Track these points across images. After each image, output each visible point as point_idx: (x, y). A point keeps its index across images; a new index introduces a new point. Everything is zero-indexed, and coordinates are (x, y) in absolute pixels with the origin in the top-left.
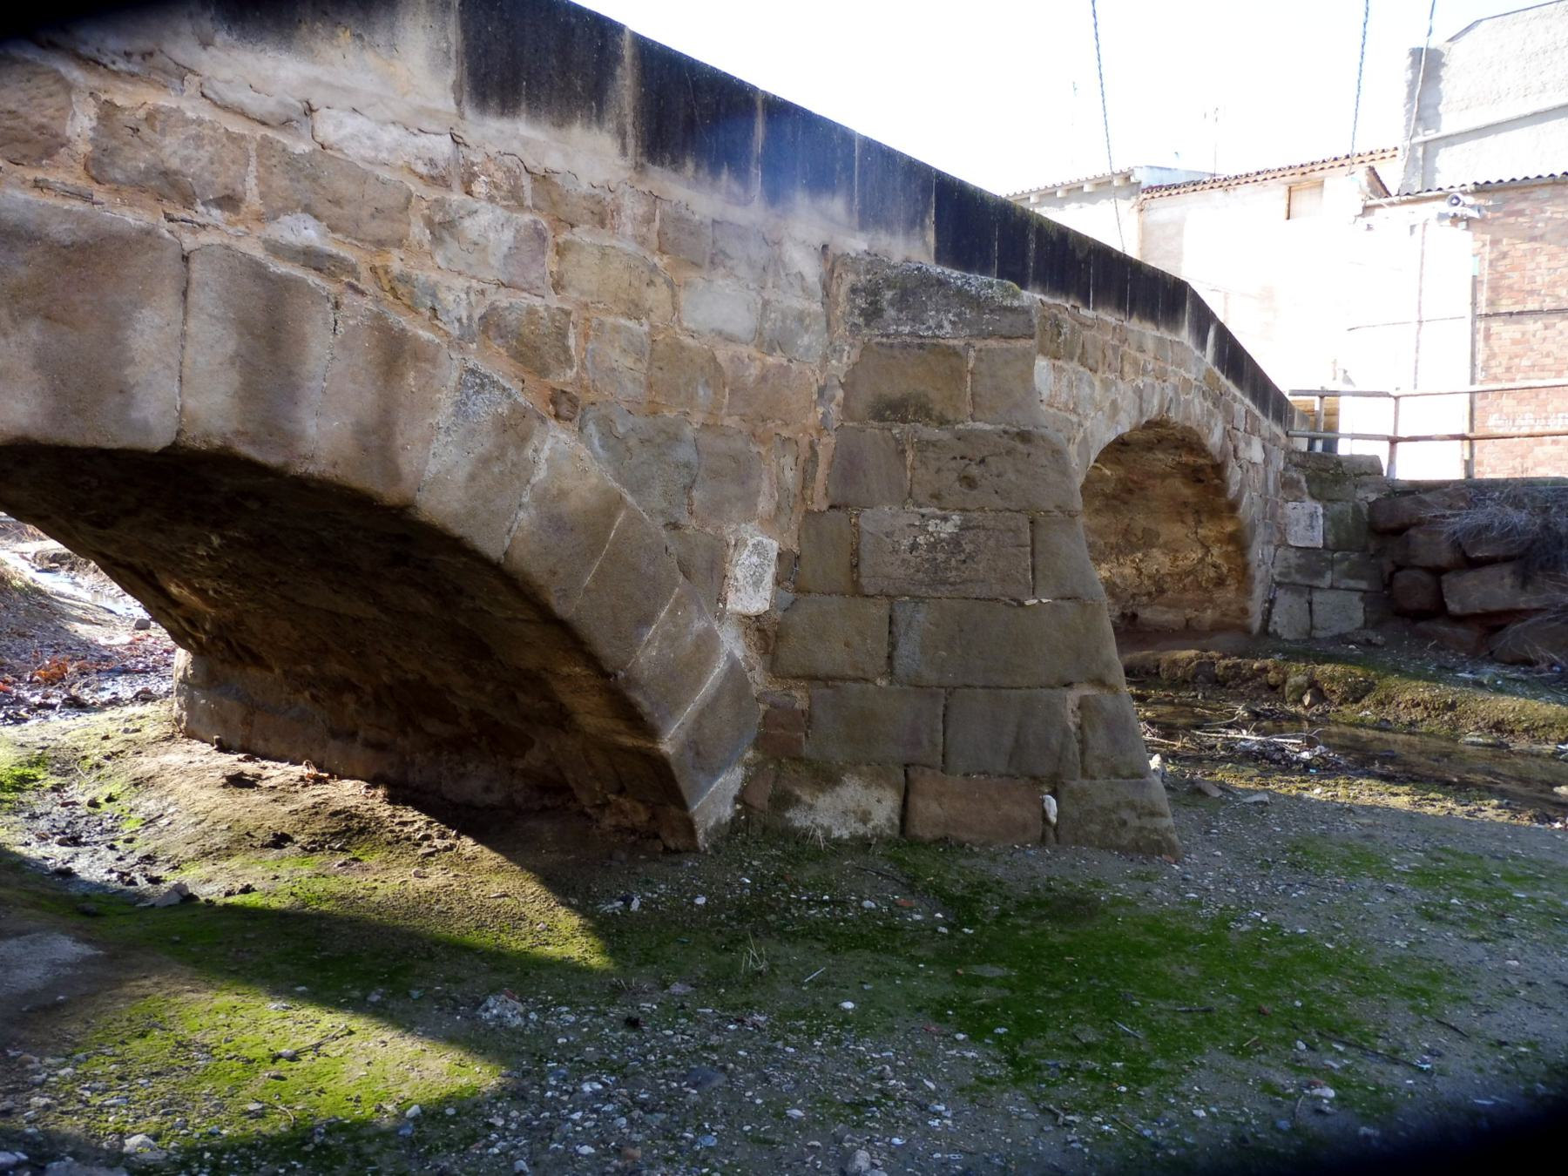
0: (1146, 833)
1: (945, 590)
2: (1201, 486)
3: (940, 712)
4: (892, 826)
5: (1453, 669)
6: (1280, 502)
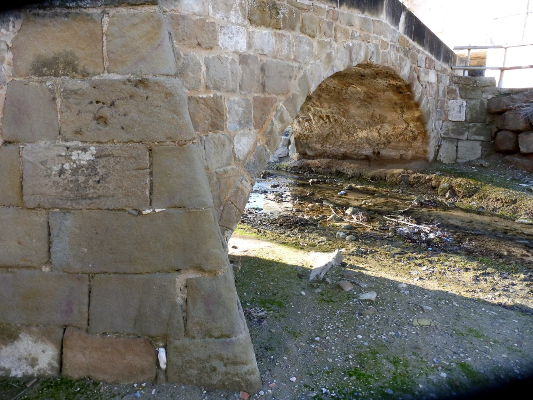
0: (230, 376)
1: (84, 203)
2: (402, 95)
3: (86, 290)
4: (52, 368)
5: (519, 181)
6: (446, 100)
